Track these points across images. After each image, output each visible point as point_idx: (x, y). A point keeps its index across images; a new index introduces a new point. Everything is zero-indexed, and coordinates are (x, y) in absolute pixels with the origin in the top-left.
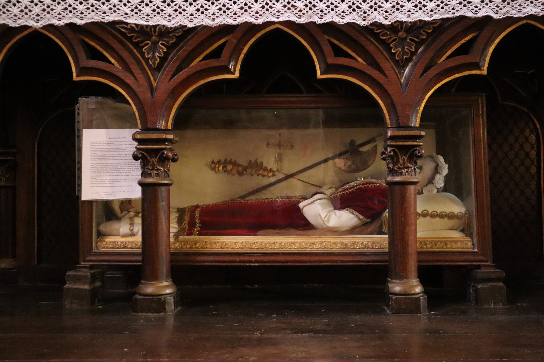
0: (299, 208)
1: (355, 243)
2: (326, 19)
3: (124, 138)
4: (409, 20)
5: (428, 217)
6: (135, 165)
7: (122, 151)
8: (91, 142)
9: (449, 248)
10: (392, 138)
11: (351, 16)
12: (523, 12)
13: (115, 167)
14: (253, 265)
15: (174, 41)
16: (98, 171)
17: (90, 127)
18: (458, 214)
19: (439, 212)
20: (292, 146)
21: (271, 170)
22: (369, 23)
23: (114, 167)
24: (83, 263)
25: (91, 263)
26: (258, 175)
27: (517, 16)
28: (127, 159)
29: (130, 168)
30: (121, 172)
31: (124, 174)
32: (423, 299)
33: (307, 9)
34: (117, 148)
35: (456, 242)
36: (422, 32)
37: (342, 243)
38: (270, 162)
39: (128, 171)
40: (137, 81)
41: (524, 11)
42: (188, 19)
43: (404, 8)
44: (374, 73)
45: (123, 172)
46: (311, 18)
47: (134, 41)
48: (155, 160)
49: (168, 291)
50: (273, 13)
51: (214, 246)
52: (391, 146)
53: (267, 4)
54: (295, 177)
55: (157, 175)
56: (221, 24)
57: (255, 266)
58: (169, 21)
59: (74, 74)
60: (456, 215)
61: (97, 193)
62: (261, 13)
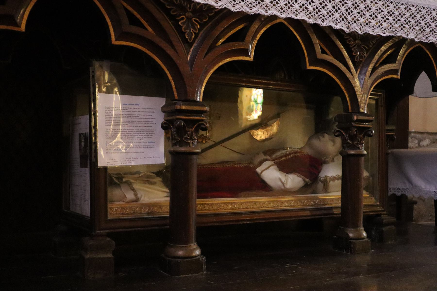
0: (257, 173)
2: (338, 27)
3: (137, 105)
4: (266, 14)
6: (147, 133)
7: (135, 118)
8: (106, 107)
12: (429, 39)
13: (129, 133)
14: (246, 223)
15: (206, 20)
16: (113, 137)
18: (337, 176)
19: (335, 176)
20: (219, 117)
22: (350, 31)
23: (127, 133)
24: (98, 232)
25: (107, 231)
27: (425, 41)
28: (140, 126)
29: (142, 135)
30: (134, 139)
31: (137, 141)
33: (272, 5)
34: (130, 115)
36: (371, 42)
39: (140, 138)
40: (177, 52)
42: (231, 3)
43: (371, 24)
45: (136, 139)
46: (316, 20)
47: (172, 13)
50: (293, 11)
53: (289, 3)
54: (223, 144)
56: (256, 13)
57: (247, 223)
59: (113, 37)
60: (335, 177)
61: (112, 159)
62: (284, 9)
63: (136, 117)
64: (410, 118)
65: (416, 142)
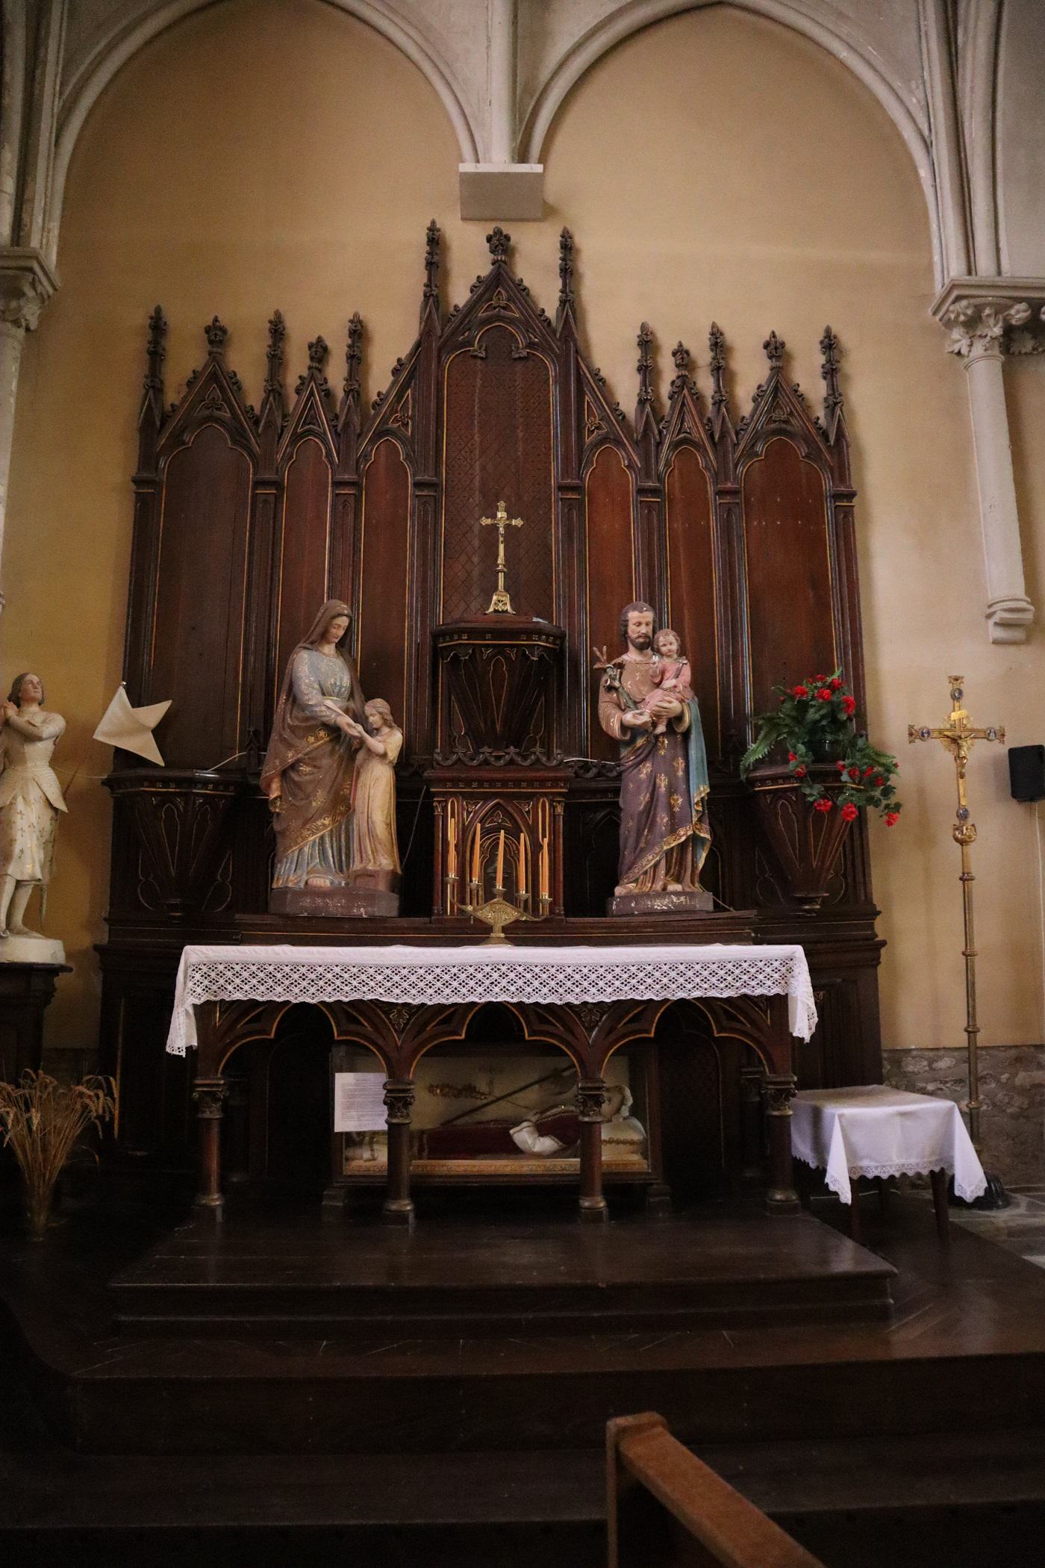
1: (555, 1165)
5: (613, 1144)
9: (629, 1169)
10: (582, 1088)
11: (550, 998)
17: (341, 1071)
21: (483, 1094)
26: (472, 1097)
32: (605, 1213)
35: (634, 1164)
37: (545, 1166)
38: (482, 1086)
41: (676, 995)
44: (570, 1038)
48: (400, 1105)
49: (409, 1208)
51: (441, 1169)
52: (581, 1095)
55: (402, 1116)
58: (414, 999)
63: (649, 822)
64: (172, 1026)
65: (925, 1063)
